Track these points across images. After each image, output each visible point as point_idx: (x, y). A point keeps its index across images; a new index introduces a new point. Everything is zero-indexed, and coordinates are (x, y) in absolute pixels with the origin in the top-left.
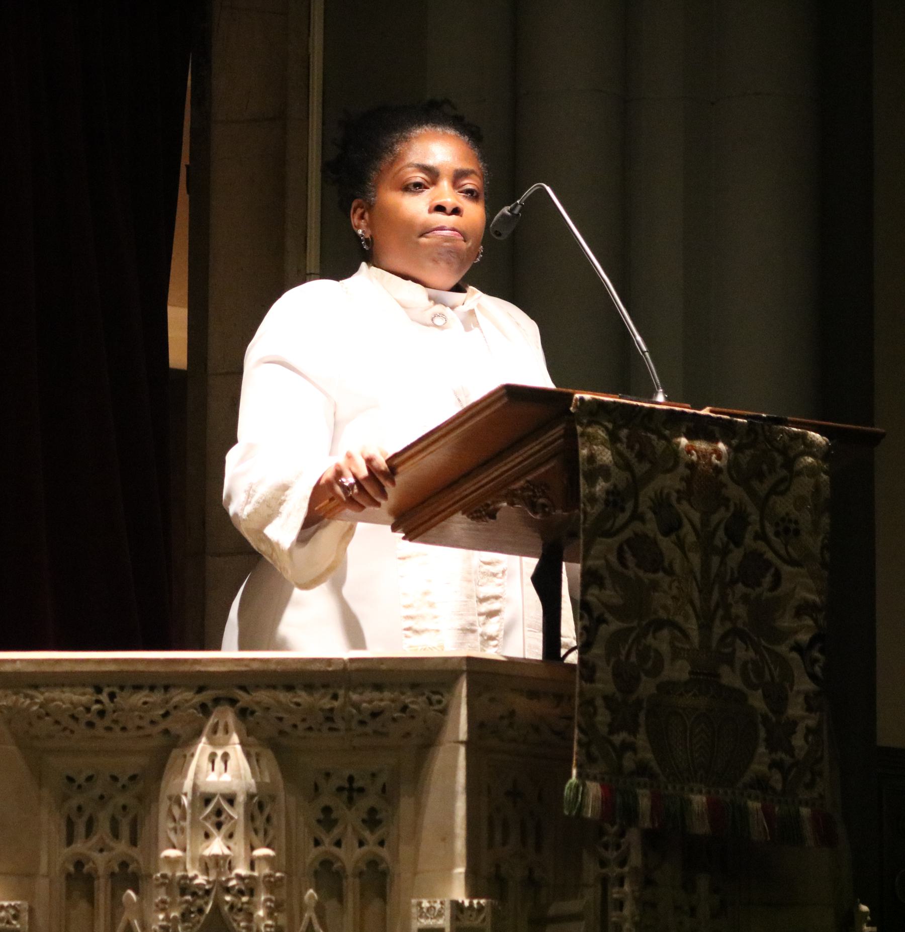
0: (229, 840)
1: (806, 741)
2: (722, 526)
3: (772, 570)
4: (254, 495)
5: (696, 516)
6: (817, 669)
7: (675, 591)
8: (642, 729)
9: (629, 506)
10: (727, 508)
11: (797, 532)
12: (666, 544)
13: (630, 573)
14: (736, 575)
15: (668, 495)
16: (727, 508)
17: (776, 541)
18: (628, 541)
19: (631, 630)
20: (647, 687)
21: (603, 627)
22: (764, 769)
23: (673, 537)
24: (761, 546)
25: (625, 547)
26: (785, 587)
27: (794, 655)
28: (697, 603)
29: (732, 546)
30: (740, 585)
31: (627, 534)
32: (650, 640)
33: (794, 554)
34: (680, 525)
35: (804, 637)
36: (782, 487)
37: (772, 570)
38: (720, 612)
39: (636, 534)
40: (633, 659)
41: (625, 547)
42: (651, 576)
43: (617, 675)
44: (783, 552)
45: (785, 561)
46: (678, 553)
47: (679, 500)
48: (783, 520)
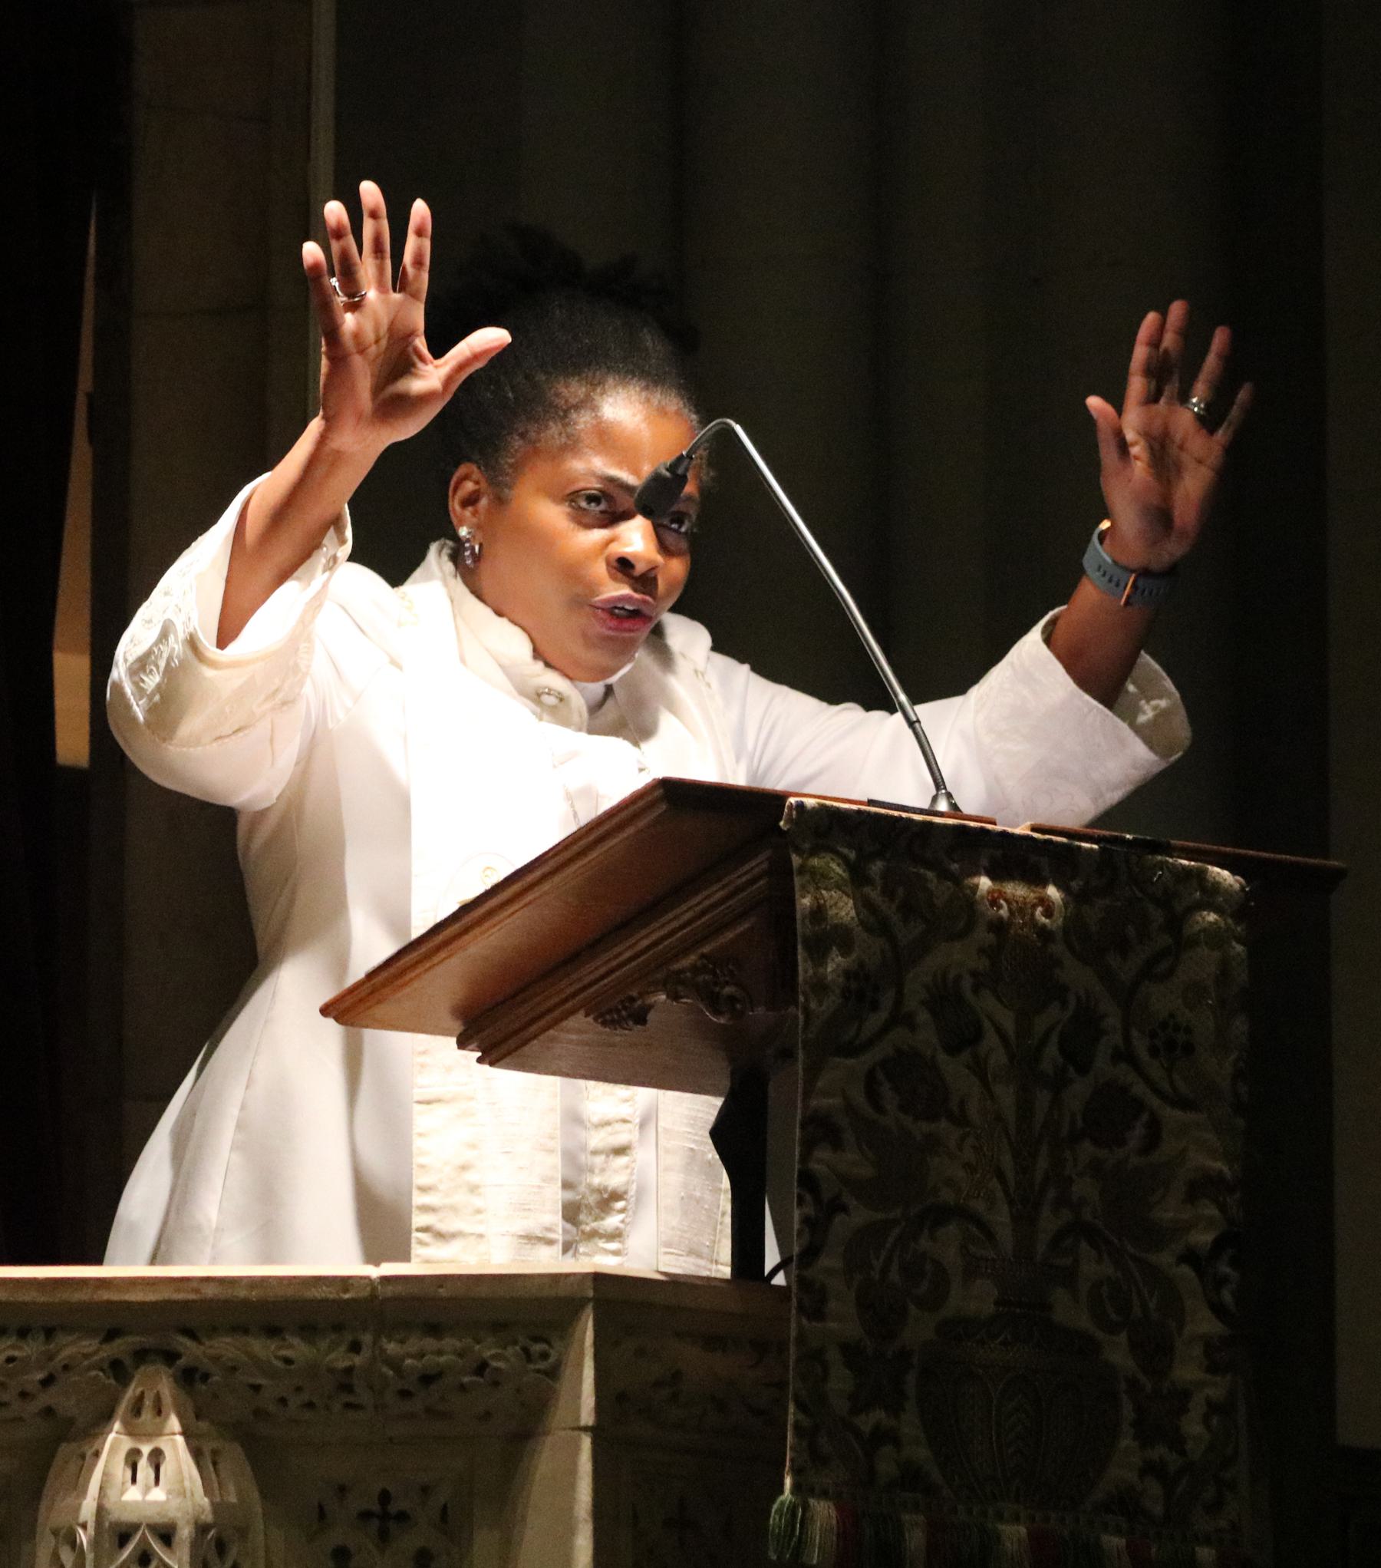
6: (1227, 1296)
9: (887, 1000)
10: (1064, 1004)
12: (954, 1069)
15: (958, 978)
16: (1064, 1004)
17: (1156, 1071)
24: (1123, 1073)
25: (880, 1076)
27: (1186, 1270)
35: (1203, 1238)
41: (880, 1076)
42: (925, 1127)
47: (976, 989)
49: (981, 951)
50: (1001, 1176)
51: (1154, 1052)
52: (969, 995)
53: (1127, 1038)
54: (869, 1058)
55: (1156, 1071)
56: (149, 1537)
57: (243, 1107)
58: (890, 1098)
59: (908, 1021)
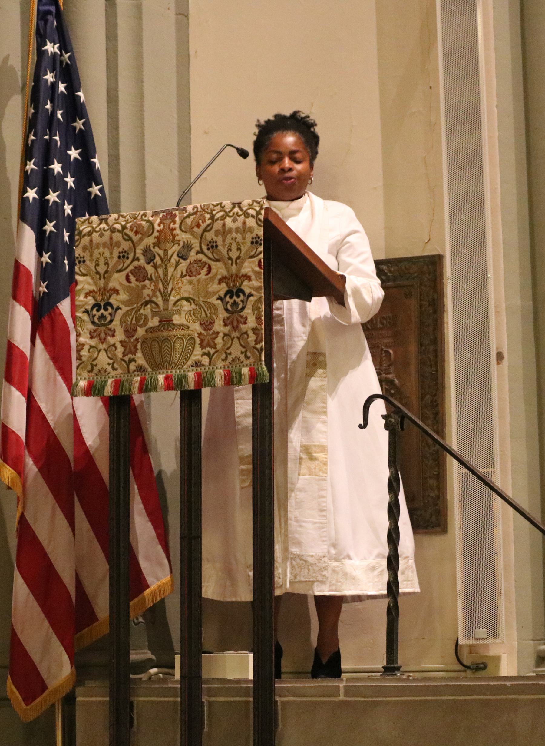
1: (223, 340)
2: (176, 254)
3: (207, 266)
5: (161, 252)
6: (229, 307)
7: (153, 287)
8: (139, 351)
9: (131, 256)
10: (179, 244)
11: (217, 246)
12: (149, 268)
13: (132, 285)
14: (185, 273)
15: (149, 246)
16: (179, 244)
17: (209, 254)
18: (131, 272)
19: (133, 309)
20: (141, 332)
22: (199, 357)
23: (152, 264)
24: (200, 256)
25: (130, 274)
26: (213, 271)
27: (219, 302)
28: (162, 290)
31: (131, 267)
32: (142, 311)
33: (216, 257)
34: (155, 257)
35: (222, 294)
36: (209, 228)
39: (135, 267)
40: (134, 322)
41: (130, 274)
42: (142, 283)
43: (126, 331)
45: (214, 261)
46: (153, 270)
47: (154, 247)
48: (210, 242)
49: (155, 237)
50: (160, 291)
51: (208, 249)
52: (152, 248)
53: (201, 247)
54: (128, 270)
55: (210, 255)
56: (284, 686)
57: (422, 453)
58: (132, 279)
59: (138, 259)
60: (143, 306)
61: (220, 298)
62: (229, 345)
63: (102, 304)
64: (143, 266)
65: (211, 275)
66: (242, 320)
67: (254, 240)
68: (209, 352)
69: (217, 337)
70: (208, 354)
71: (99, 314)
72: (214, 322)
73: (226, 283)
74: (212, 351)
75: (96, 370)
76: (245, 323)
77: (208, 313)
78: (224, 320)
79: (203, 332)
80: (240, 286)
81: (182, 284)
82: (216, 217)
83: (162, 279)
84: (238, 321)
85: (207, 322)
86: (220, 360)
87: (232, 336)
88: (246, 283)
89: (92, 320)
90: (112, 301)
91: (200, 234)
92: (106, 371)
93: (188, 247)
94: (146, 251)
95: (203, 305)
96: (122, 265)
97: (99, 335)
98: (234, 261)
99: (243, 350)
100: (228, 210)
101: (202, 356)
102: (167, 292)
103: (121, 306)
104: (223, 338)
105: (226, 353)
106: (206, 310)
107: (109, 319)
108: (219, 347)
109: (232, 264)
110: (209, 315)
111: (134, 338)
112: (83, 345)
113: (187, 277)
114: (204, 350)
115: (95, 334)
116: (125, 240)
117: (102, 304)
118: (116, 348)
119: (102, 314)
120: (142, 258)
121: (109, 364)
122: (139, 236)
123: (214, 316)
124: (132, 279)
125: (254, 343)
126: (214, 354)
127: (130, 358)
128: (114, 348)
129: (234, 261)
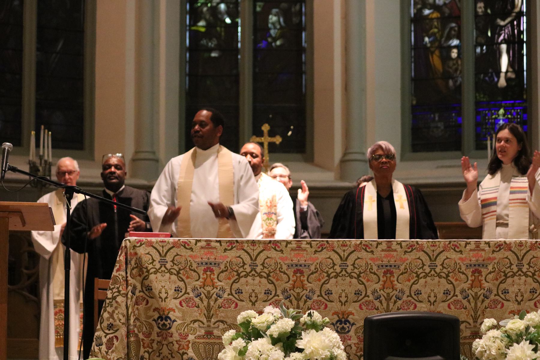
0: (503, 169)
3: (146, 300)
4: (54, 309)
8: (191, 348)
21: (175, 323)
28: (206, 315)
29: (133, 296)
30: (136, 305)
36: (146, 278)
37: (146, 300)
38: (133, 314)
44: (238, 298)
47: (380, 291)
49: (469, 284)
60: (192, 323)
61: (154, 320)
62: (161, 348)
63: (343, 320)
64: (460, 300)
65: (148, 306)
66: (170, 335)
67: (177, 289)
68: (148, 350)
69: (153, 342)
70: (148, 352)
71: (341, 326)
72: (151, 334)
73: (158, 312)
74: (150, 350)
75: (161, 356)
76: (171, 337)
77: (148, 328)
78: (157, 333)
79: (144, 338)
80: (168, 315)
81: (219, 312)
82: (508, 275)
83: (474, 309)
84: (166, 335)
85: (147, 333)
86: (156, 356)
87: (163, 343)
88: (172, 313)
89: (158, 326)
90: (170, 315)
91: (498, 284)
92: (167, 357)
93: (490, 291)
94: (374, 292)
95: (144, 323)
96: (177, 295)
97: (163, 335)
98: (163, 299)
99: (170, 352)
100: (158, 268)
101: (144, 353)
102: (477, 317)
103: (176, 320)
104: (157, 343)
105: (159, 352)
106: (146, 326)
107: (168, 326)
108: (155, 348)
109: (162, 301)
110: (148, 329)
111: (187, 340)
112: (154, 340)
113: (488, 309)
114: (145, 349)
115: (160, 334)
116: (270, 283)
117: (343, 320)
118: (351, 348)
119: (343, 326)
120: (371, 296)
121: (169, 354)
122: (458, 282)
123: (151, 330)
124: (452, 306)
125: (177, 349)
126: (151, 352)
127: (183, 352)
128: (172, 344)
129: (163, 299)
